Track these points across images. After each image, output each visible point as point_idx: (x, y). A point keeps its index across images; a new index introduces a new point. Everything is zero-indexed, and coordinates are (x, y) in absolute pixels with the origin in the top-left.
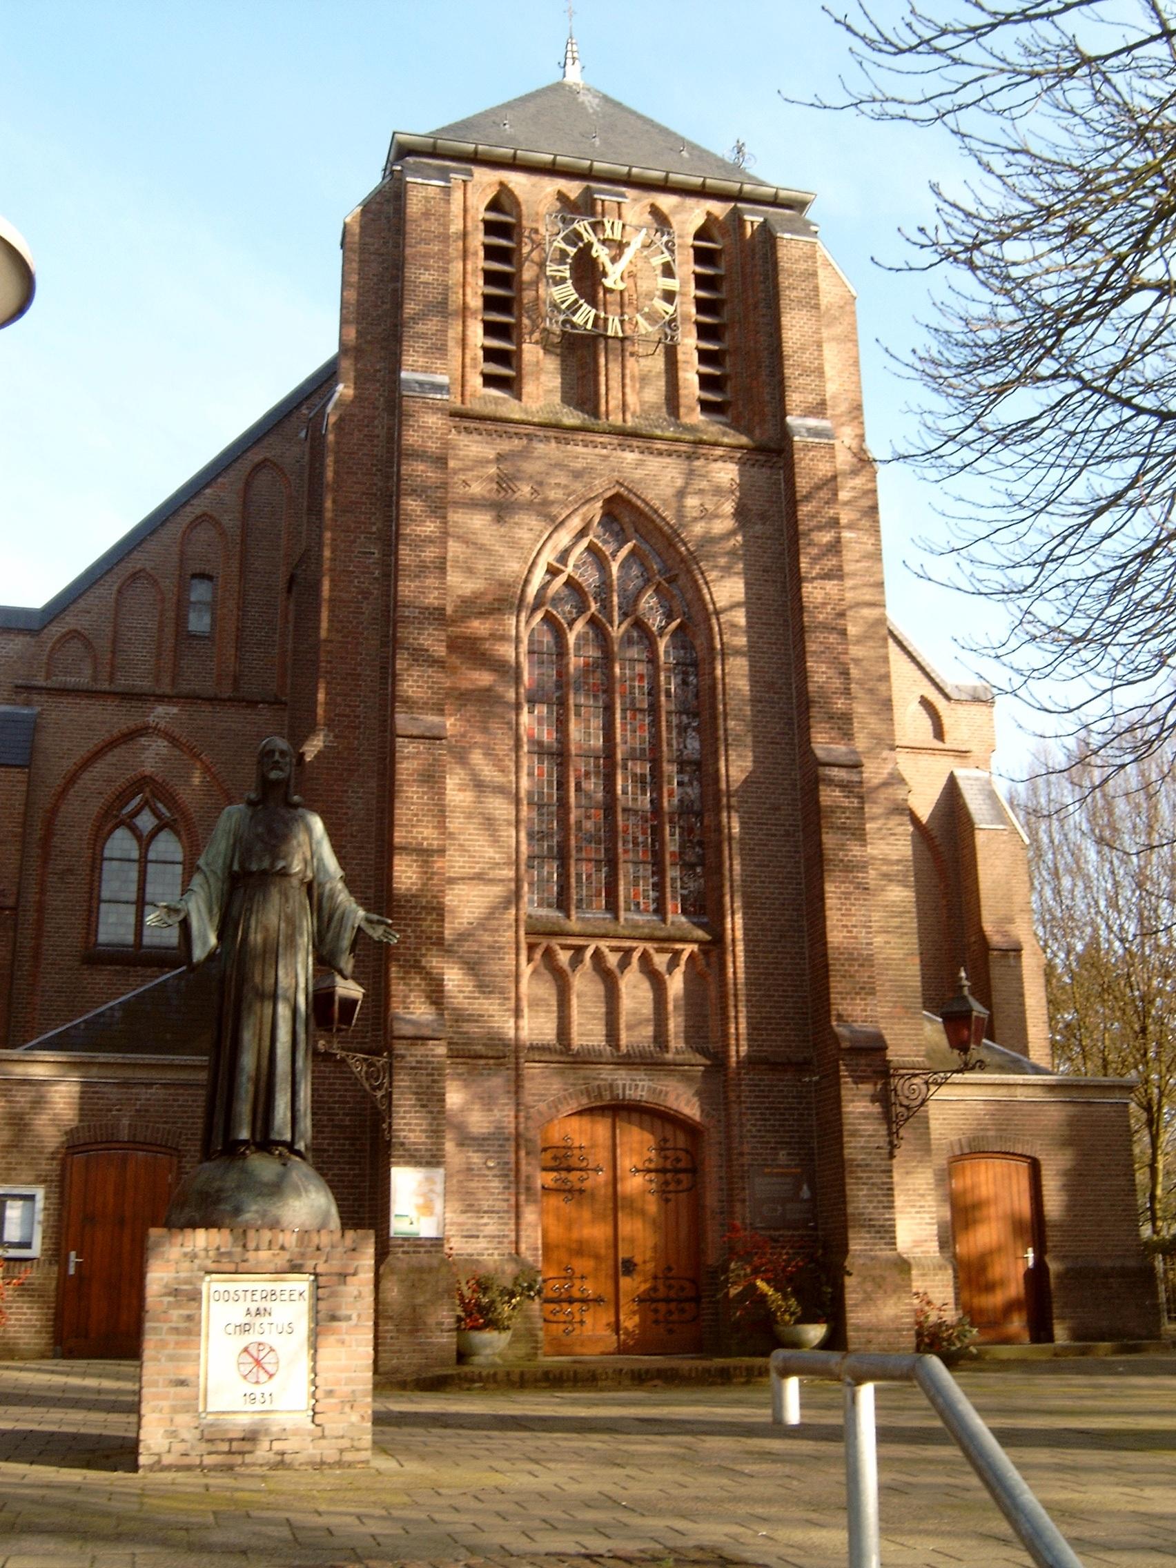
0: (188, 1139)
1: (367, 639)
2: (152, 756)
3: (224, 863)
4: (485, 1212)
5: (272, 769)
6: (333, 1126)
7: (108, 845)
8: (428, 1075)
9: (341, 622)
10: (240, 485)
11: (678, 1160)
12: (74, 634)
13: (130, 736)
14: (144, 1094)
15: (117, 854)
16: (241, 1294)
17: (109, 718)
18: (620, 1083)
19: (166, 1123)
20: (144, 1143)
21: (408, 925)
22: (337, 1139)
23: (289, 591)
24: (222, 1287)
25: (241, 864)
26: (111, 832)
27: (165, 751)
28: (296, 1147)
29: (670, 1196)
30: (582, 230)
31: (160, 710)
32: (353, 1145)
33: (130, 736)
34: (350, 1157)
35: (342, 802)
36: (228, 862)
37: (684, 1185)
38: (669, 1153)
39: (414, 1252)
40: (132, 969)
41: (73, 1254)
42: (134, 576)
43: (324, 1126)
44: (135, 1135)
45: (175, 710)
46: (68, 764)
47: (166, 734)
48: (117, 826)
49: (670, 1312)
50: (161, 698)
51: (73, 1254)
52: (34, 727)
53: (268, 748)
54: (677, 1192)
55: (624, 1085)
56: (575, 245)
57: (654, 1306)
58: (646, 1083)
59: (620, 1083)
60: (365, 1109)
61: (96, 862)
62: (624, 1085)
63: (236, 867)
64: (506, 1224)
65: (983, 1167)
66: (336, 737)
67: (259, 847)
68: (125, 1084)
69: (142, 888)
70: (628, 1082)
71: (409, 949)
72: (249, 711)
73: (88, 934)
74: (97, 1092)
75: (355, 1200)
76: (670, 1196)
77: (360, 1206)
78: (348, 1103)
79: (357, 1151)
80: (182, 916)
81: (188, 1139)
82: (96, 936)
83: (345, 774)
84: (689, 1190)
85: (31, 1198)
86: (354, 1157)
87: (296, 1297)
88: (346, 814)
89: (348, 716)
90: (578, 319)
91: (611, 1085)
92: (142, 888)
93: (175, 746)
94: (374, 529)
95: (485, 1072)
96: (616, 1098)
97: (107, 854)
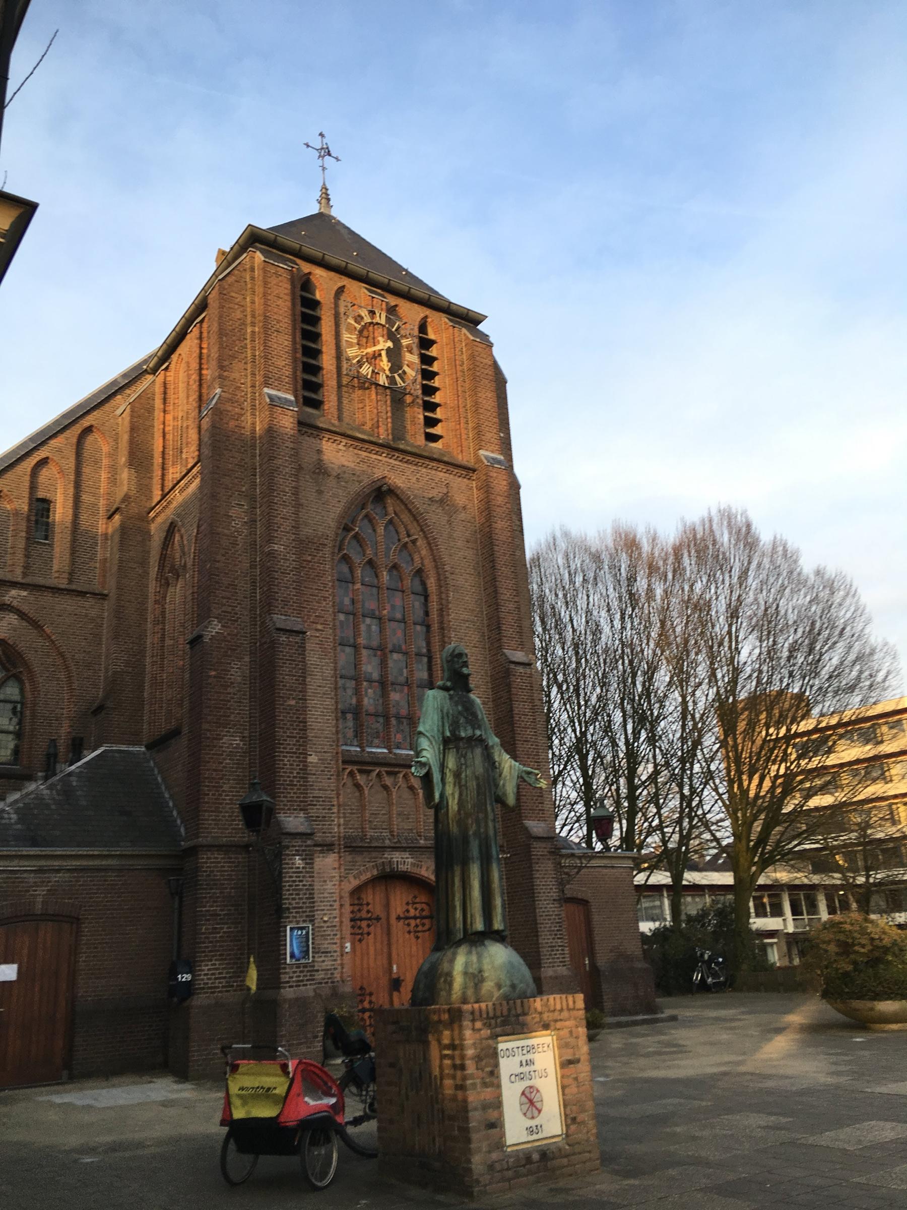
3: (438, 731)
4: (323, 953)
10: (75, 440)
11: (422, 910)
14: (55, 878)
18: (395, 860)
19: (69, 898)
22: (226, 906)
24: (510, 1045)
27: (16, 622)
29: (420, 934)
30: (363, 315)
31: (14, 592)
36: (441, 729)
37: (427, 927)
38: (418, 906)
43: (218, 897)
45: (25, 593)
47: (18, 610)
50: (14, 585)
53: (457, 652)
54: (424, 931)
56: (359, 323)
58: (410, 860)
59: (395, 860)
63: (448, 734)
64: (335, 960)
65: (398, 893)
66: (222, 626)
67: (462, 720)
68: (40, 871)
72: (79, 598)
75: (238, 949)
77: (241, 954)
78: (233, 880)
83: (229, 652)
84: (429, 930)
93: (23, 619)
94: (244, 489)
96: (392, 870)
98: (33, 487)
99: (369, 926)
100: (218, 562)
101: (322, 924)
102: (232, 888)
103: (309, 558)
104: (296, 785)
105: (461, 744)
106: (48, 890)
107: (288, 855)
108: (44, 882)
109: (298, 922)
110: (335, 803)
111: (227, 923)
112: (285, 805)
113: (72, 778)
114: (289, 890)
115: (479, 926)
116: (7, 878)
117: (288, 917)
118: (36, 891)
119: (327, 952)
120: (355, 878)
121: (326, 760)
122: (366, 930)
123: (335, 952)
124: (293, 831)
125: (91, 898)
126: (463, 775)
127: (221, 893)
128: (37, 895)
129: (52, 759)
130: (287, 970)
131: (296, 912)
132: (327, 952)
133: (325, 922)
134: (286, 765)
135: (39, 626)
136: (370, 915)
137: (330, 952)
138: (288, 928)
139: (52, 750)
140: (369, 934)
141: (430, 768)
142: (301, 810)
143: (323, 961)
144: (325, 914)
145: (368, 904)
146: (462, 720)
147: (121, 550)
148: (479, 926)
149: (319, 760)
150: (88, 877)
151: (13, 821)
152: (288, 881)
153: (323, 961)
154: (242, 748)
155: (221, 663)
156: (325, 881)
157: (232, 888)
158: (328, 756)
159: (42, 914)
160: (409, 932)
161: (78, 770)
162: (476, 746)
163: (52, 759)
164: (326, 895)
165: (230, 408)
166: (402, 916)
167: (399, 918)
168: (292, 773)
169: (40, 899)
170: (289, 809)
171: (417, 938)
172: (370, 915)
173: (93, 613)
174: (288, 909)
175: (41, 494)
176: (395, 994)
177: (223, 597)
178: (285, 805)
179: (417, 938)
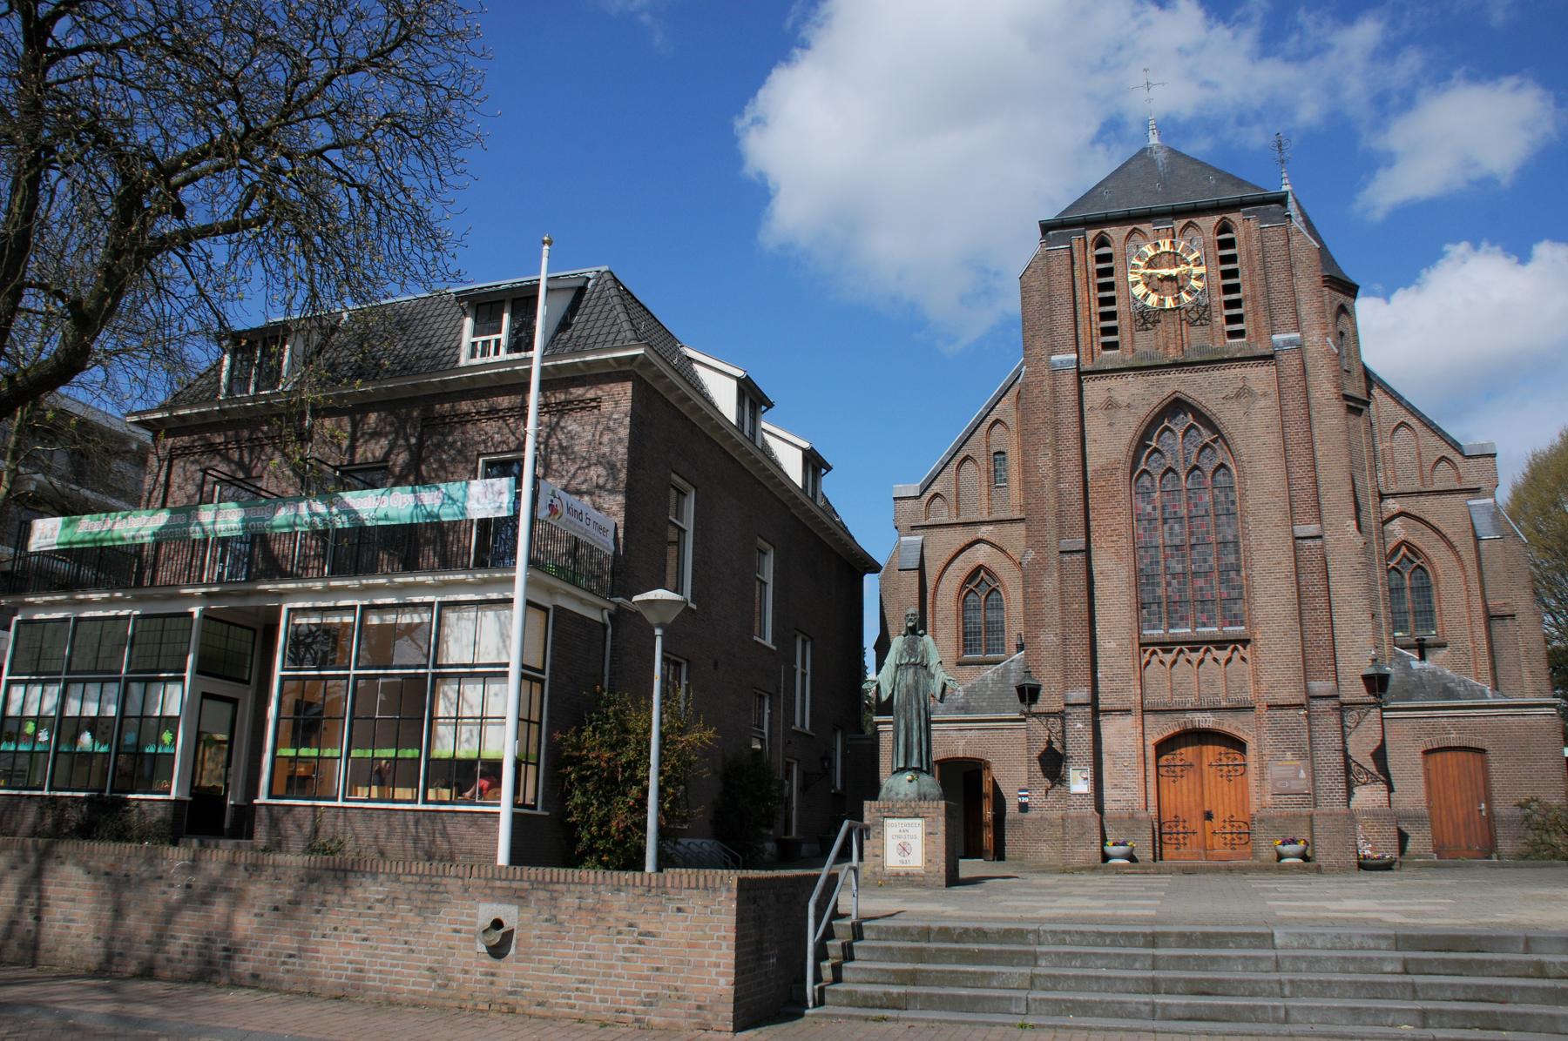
2: (981, 555)
12: (936, 495)
13: (971, 545)
17: (960, 537)
33: (971, 545)
42: (966, 458)
46: (941, 564)
90: (1149, 303)
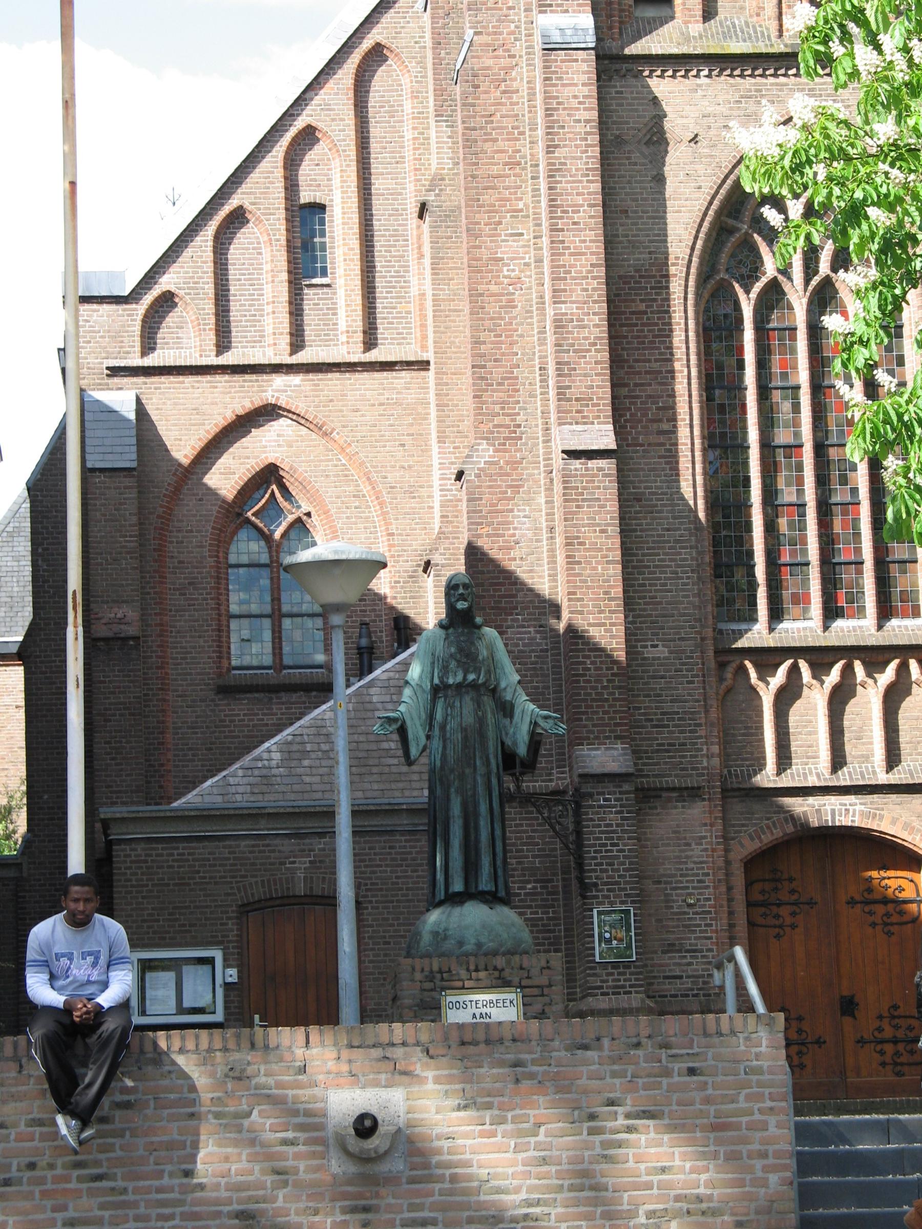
0: (367, 890)
1: (522, 336)
4: (688, 951)
5: (458, 600)
6: (523, 869)
7: (233, 548)
8: (616, 813)
9: (492, 319)
15: (244, 559)
16: (469, 1004)
18: (828, 808)
20: (322, 897)
21: (589, 657)
23: (421, 216)
25: (441, 679)
26: (235, 533)
28: (499, 895)
32: (546, 887)
34: (542, 900)
35: (509, 523)
39: (614, 994)
40: (273, 696)
41: (257, 1017)
44: (311, 888)
48: (240, 527)
49: (897, 1053)
51: (257, 1017)
52: (767, 1179)
55: (833, 811)
57: (879, 1048)
59: (828, 808)
60: (555, 849)
61: (222, 570)
62: (833, 811)
63: (436, 681)
66: (496, 451)
69: (276, 600)
70: (837, 808)
71: (589, 681)
73: (220, 657)
74: (268, 845)
76: (892, 929)
79: (549, 894)
80: (399, 723)
81: (367, 890)
82: (229, 658)
85: (210, 961)
86: (547, 900)
87: (508, 1004)
88: (514, 535)
89: (508, 426)
91: (818, 811)
92: (276, 600)
95: (680, 804)
97: (232, 559)
98: (291, 186)
99: (793, 914)
100: (484, 343)
101: (686, 910)
102: (534, 857)
103: (642, 307)
104: (607, 700)
105: (450, 692)
106: (310, 862)
107: (592, 807)
108: (304, 850)
109: (612, 903)
110: (703, 721)
111: (530, 907)
112: (588, 732)
113: (373, 691)
114: (595, 858)
115: (458, 886)
116: (253, 846)
117: (596, 897)
118: (294, 862)
119: (695, 951)
120: (752, 839)
121: (684, 651)
122: (789, 920)
123: (711, 950)
124: (599, 771)
125: (374, 872)
126: (448, 727)
127: (519, 863)
128: (297, 869)
129: (366, 656)
130: (598, 971)
131: (608, 890)
132: (695, 951)
133: (690, 906)
134: (589, 669)
135: (325, 434)
136: (794, 897)
137: (701, 951)
138: (595, 911)
139: (364, 642)
140: (793, 927)
141: (404, 722)
142: (616, 738)
143: (690, 964)
144: (690, 894)
145: (791, 880)
146: (453, 664)
147: (436, 281)
148: (458, 886)
149: (670, 652)
150: (365, 842)
151: (274, 763)
152: (594, 845)
153: (690, 964)
154: (539, 644)
155: (497, 512)
156: (689, 845)
157: (534, 857)
158: (688, 646)
159: (305, 896)
160: (874, 925)
161: (385, 676)
162: (467, 693)
163: (366, 656)
164: (691, 866)
165: (490, 62)
166: (858, 898)
167: (852, 902)
168: (600, 681)
169: (301, 875)
170: (597, 738)
171: (889, 934)
172: (794, 897)
173: (410, 397)
174: (596, 885)
175: (305, 197)
176: (847, 1020)
177: (494, 403)
178: (588, 732)
179: (889, 934)
